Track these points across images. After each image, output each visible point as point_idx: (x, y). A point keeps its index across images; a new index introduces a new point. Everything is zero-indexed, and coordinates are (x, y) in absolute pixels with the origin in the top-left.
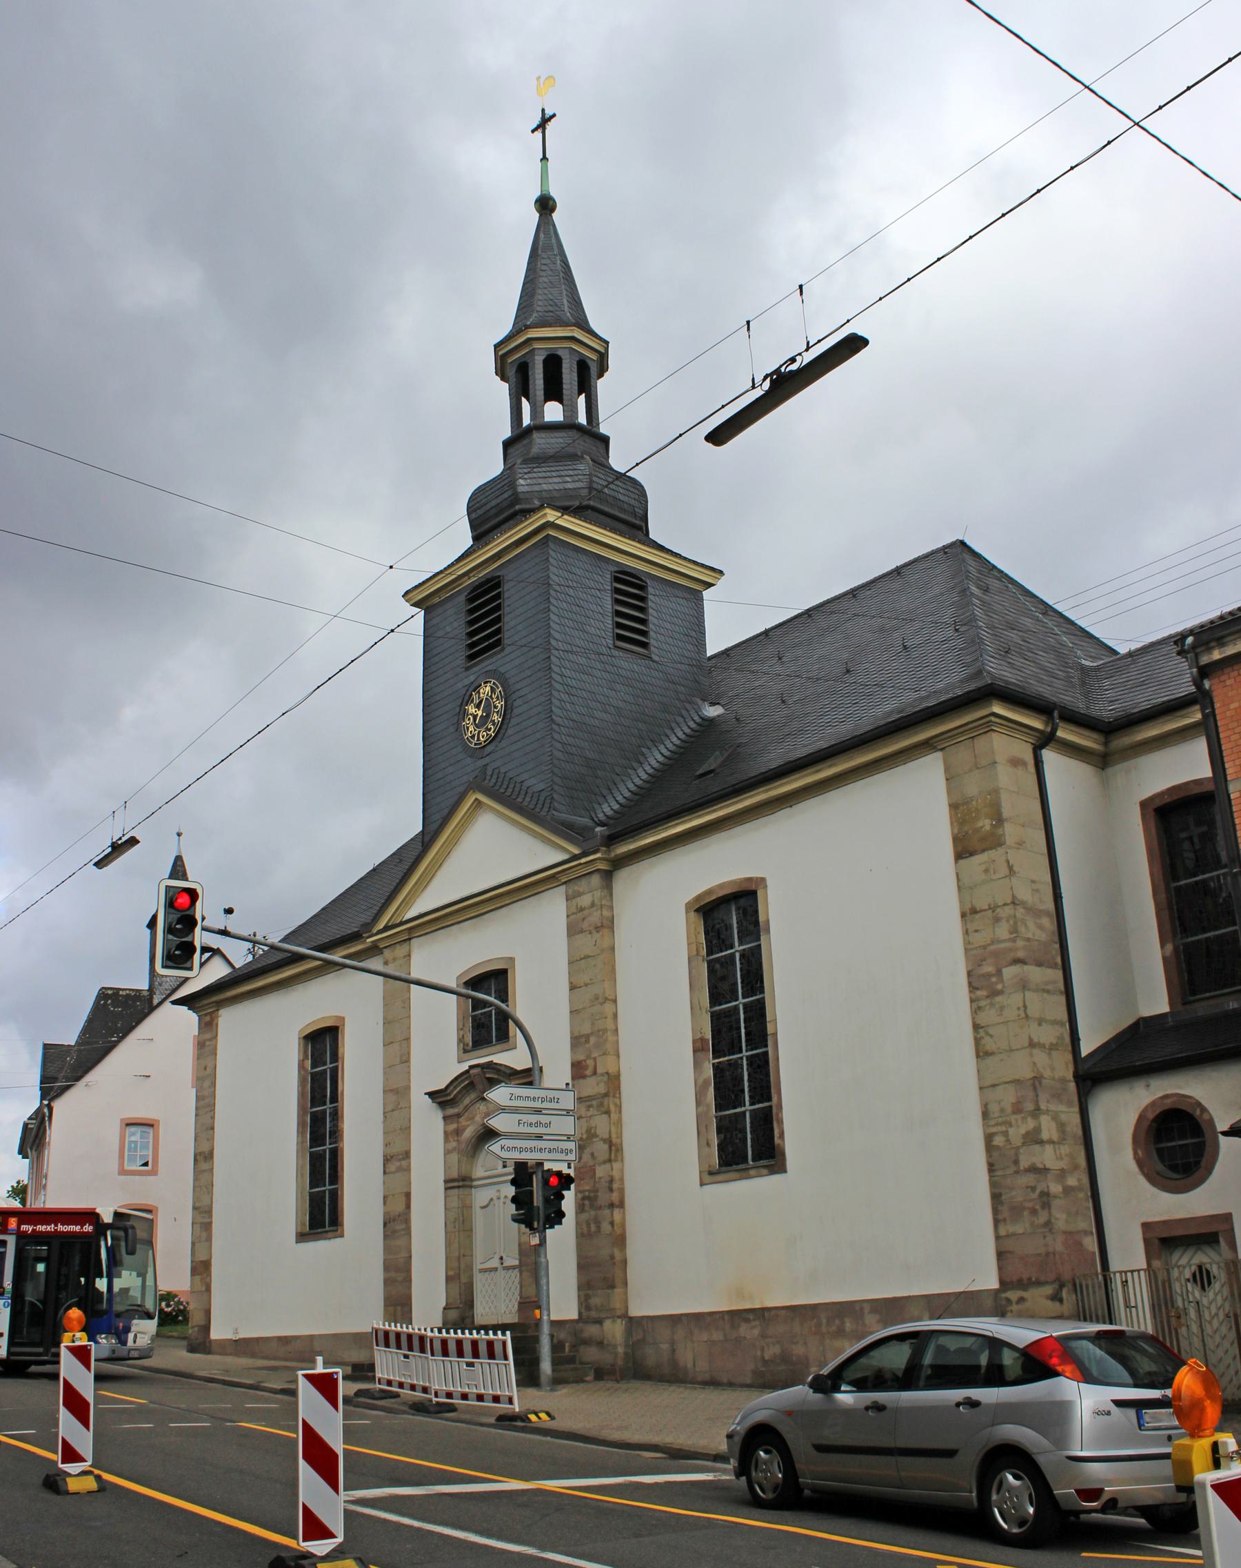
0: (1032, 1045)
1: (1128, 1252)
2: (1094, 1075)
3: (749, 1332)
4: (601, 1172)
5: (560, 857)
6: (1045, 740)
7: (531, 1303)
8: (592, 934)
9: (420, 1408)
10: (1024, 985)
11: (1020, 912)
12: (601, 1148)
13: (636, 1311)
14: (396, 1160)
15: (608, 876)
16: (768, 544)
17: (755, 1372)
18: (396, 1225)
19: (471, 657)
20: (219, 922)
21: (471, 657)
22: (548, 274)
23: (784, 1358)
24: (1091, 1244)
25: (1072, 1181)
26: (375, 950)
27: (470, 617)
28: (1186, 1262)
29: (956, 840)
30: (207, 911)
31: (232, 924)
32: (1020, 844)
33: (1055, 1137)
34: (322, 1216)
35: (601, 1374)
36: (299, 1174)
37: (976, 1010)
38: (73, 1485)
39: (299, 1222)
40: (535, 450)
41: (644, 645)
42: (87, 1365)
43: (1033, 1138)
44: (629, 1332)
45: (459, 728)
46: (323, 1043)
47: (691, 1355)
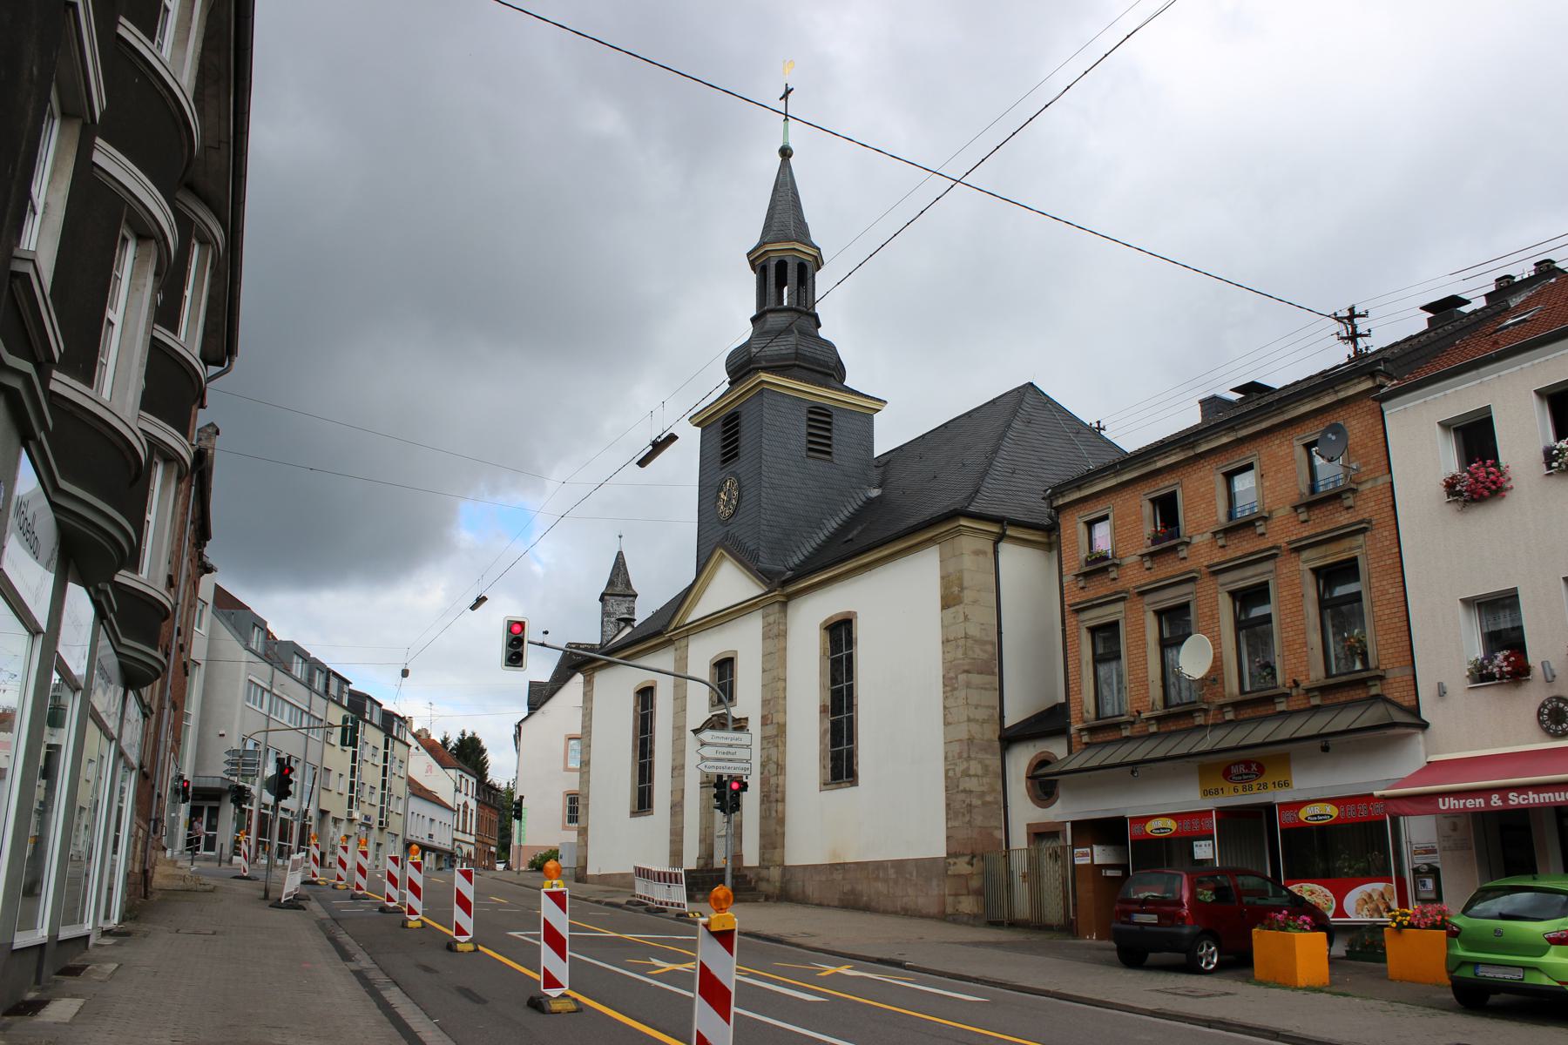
0: (969, 720)
1: (1019, 840)
2: (1010, 738)
3: (838, 876)
4: (773, 780)
5: (760, 592)
6: (1000, 538)
7: (738, 857)
8: (776, 637)
9: (649, 910)
10: (968, 685)
11: (970, 642)
12: (773, 767)
13: (788, 862)
14: (678, 769)
15: (784, 604)
16: (907, 386)
17: (840, 900)
18: (677, 807)
19: (724, 462)
20: (540, 638)
21: (724, 462)
22: (785, 203)
23: (853, 891)
24: (1001, 835)
25: (989, 798)
26: (670, 642)
27: (725, 432)
28: (1048, 846)
29: (943, 598)
30: (531, 634)
31: (547, 640)
32: (975, 602)
33: (980, 772)
34: (643, 803)
35: (767, 898)
36: (633, 776)
37: (945, 698)
38: (410, 924)
39: (633, 806)
40: (767, 326)
41: (829, 453)
42: (470, 881)
43: (966, 774)
44: (783, 875)
45: (716, 507)
46: (646, 695)
47: (812, 889)
